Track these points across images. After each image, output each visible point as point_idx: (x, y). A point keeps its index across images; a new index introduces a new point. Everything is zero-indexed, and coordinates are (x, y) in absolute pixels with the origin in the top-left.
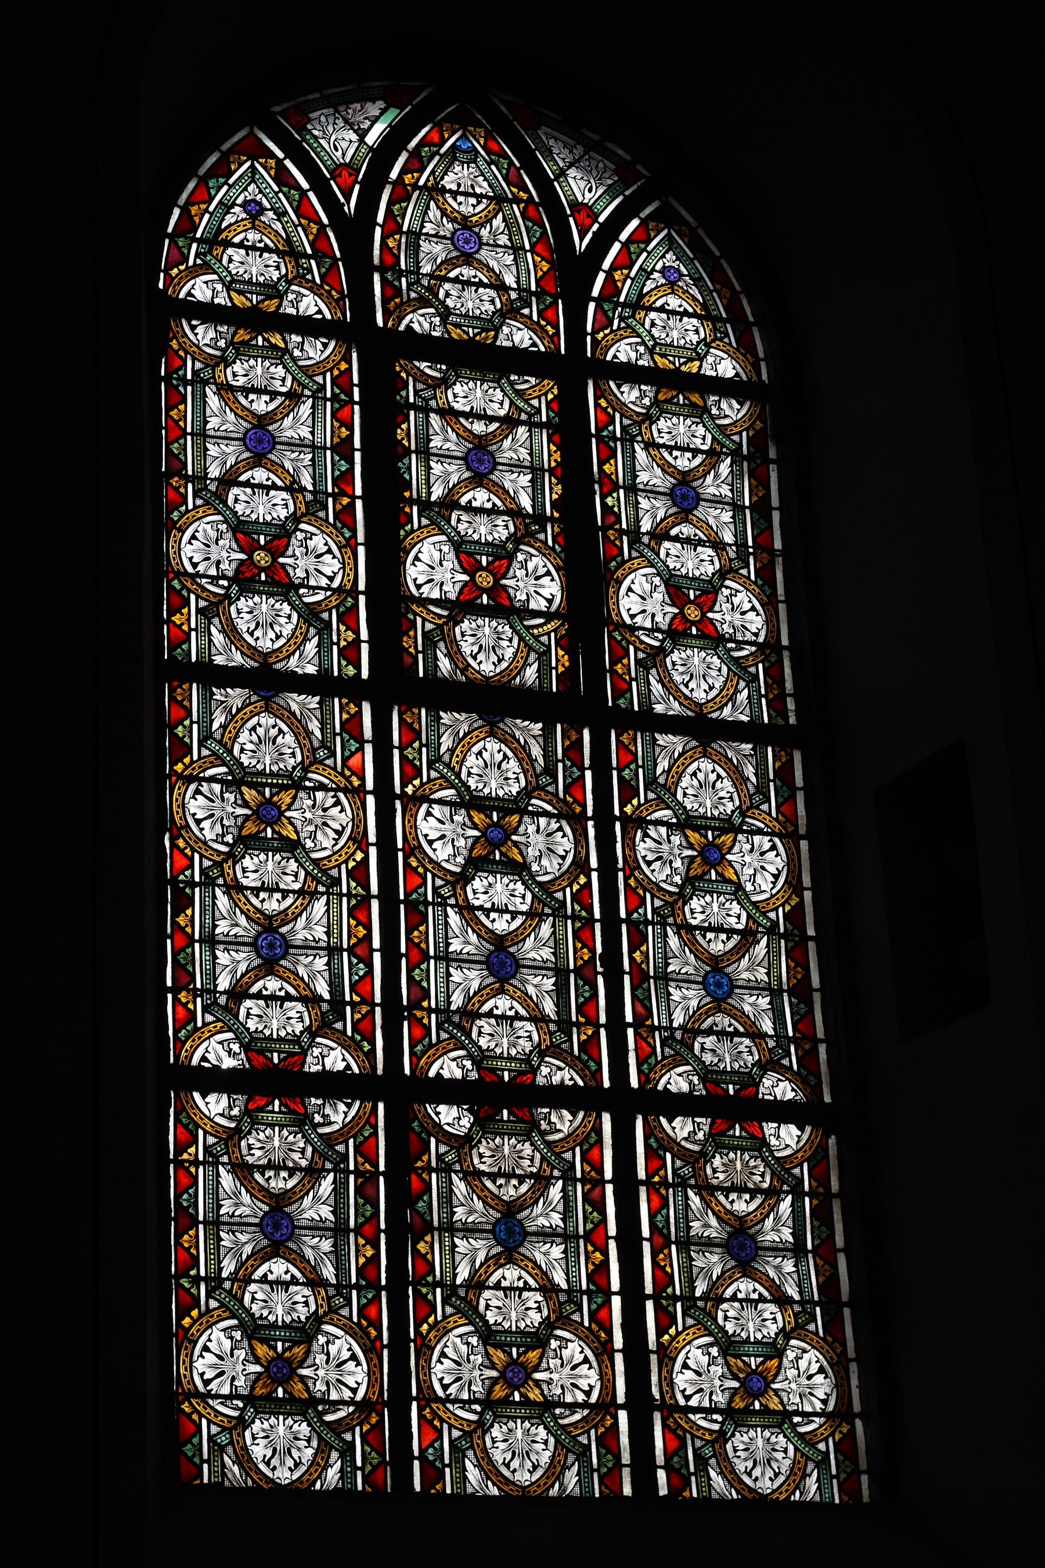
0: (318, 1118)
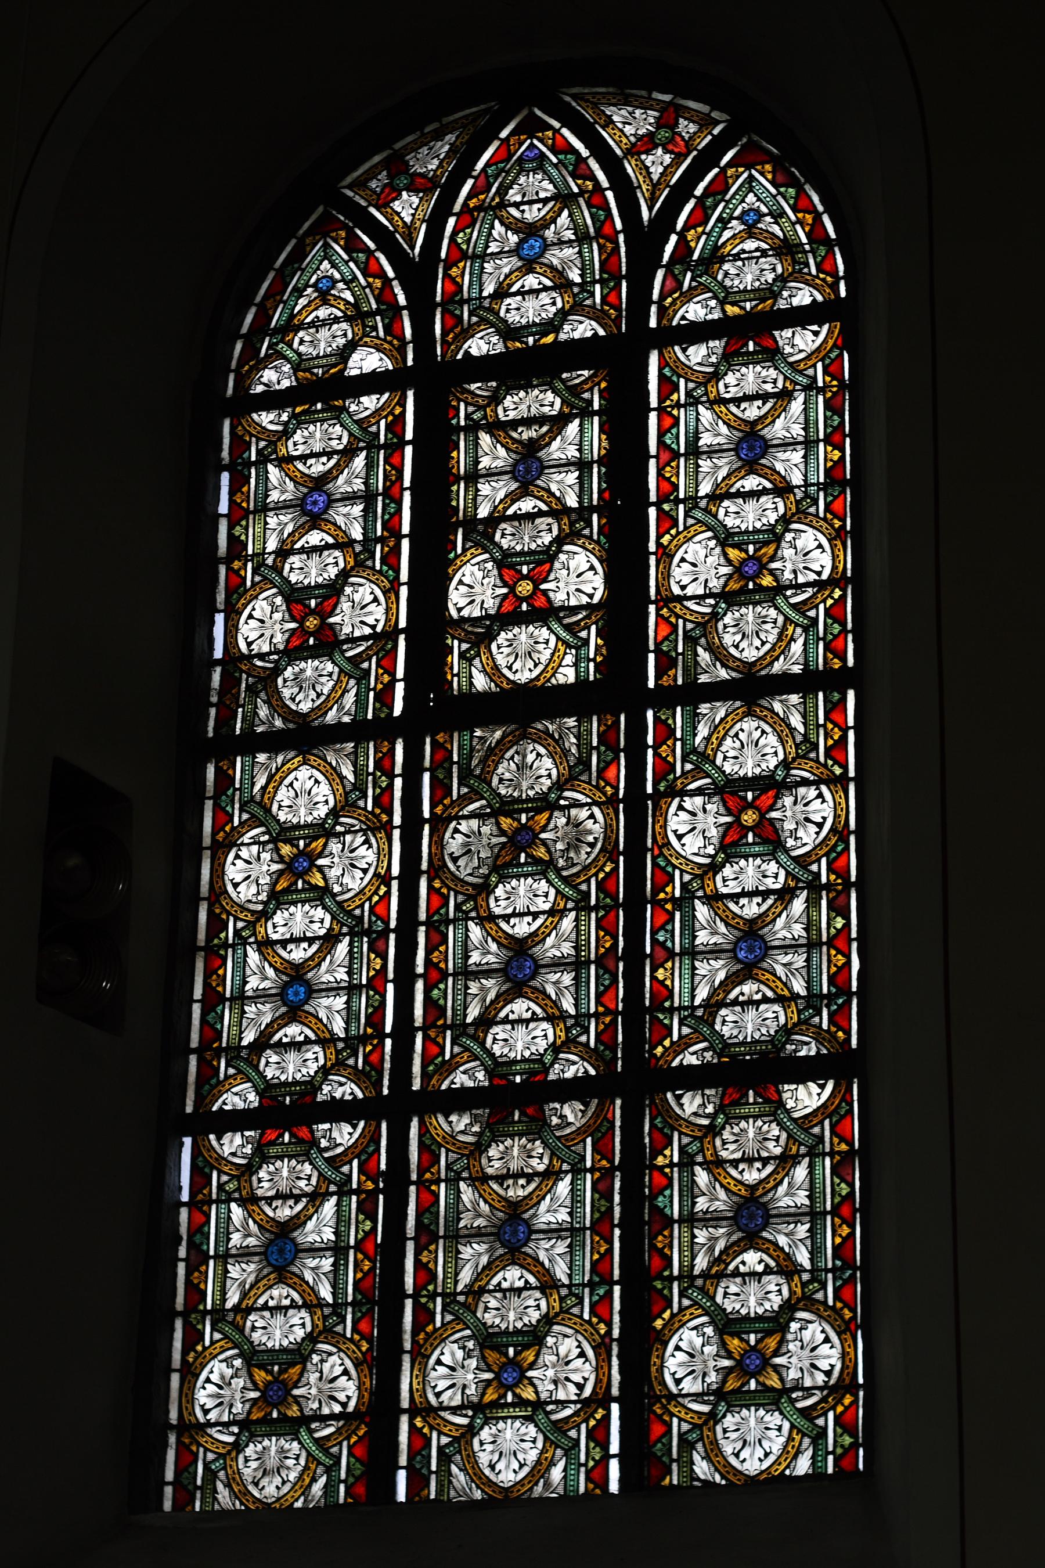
0: (324, 1143)
